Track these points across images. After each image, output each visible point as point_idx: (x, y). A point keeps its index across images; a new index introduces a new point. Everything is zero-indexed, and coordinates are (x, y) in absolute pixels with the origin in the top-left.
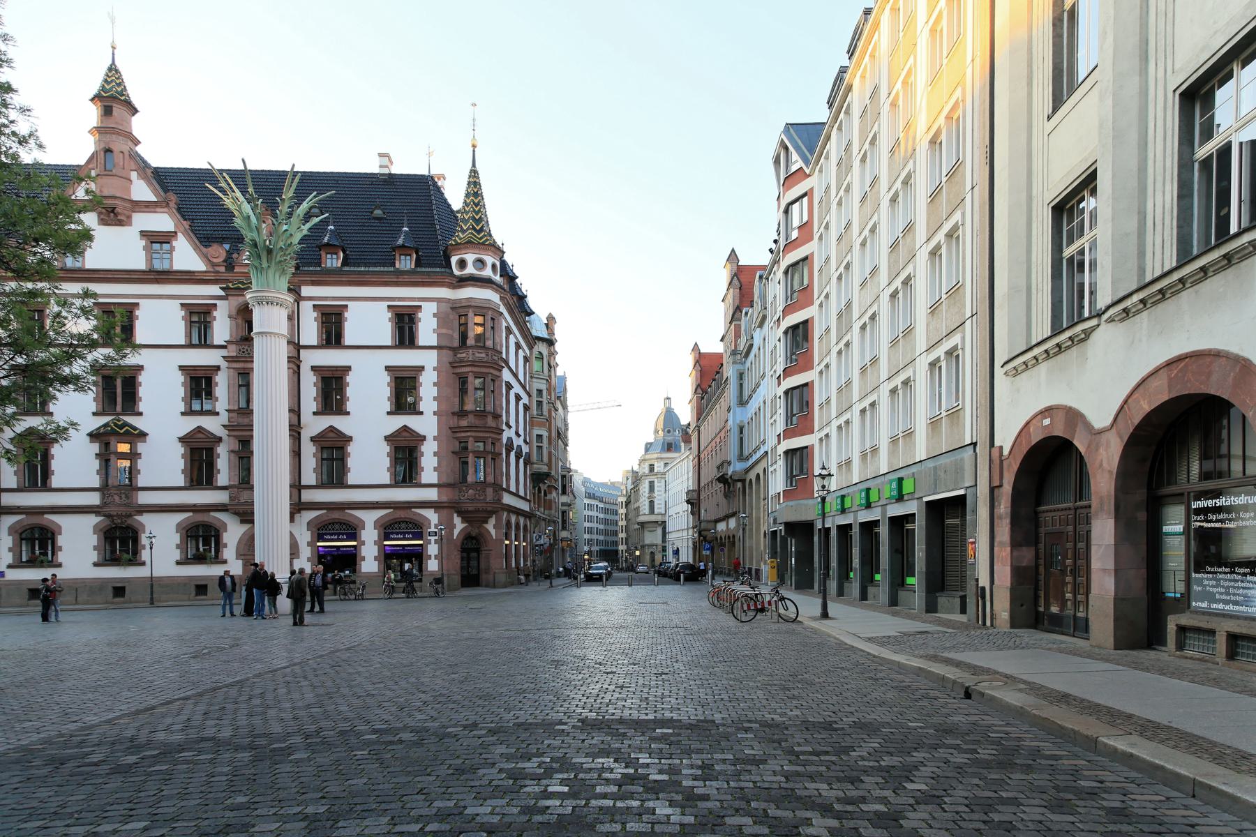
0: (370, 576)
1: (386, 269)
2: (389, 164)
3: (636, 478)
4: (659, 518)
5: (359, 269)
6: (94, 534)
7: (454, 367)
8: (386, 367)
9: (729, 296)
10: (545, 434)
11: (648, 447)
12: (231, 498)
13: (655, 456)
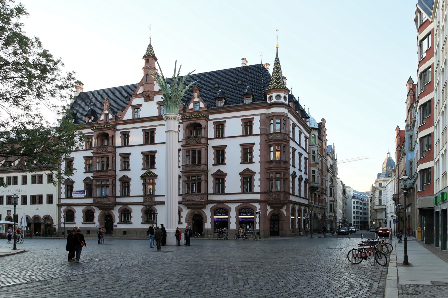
0: (208, 230)
1: (240, 104)
2: (246, 63)
3: (374, 189)
4: (384, 207)
5: (230, 106)
6: (235, 211)
7: (267, 142)
8: (240, 144)
9: (408, 100)
10: (316, 170)
11: (379, 175)
12: (183, 199)
13: (382, 179)
